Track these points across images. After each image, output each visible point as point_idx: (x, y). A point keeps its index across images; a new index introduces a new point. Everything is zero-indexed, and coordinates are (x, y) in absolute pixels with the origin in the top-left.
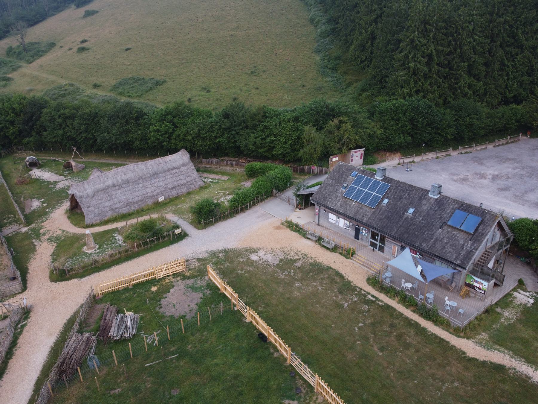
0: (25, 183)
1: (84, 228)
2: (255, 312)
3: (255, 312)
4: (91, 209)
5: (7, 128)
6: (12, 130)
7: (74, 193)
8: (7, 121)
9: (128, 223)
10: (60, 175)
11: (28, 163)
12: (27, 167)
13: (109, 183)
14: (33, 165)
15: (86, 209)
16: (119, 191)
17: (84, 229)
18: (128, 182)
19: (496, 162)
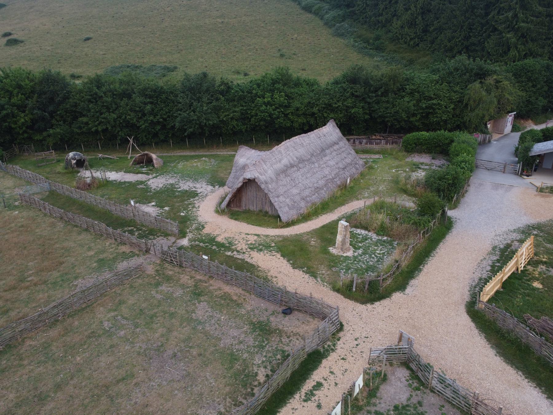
0: (94, 187)
1: (282, 227)
2: (489, 282)
3: (489, 282)
4: (281, 199)
5: (14, 116)
6: (23, 118)
7: (256, 176)
8: (14, 105)
9: (366, 204)
10: (137, 173)
11: (74, 162)
12: (73, 168)
13: (285, 161)
14: (80, 164)
15: (276, 199)
16: (299, 173)
17: (283, 230)
18: (303, 161)
19: (246, 187)
